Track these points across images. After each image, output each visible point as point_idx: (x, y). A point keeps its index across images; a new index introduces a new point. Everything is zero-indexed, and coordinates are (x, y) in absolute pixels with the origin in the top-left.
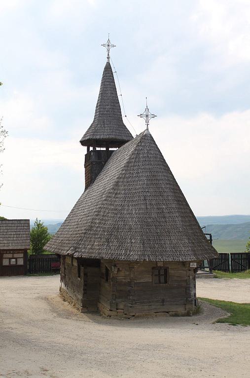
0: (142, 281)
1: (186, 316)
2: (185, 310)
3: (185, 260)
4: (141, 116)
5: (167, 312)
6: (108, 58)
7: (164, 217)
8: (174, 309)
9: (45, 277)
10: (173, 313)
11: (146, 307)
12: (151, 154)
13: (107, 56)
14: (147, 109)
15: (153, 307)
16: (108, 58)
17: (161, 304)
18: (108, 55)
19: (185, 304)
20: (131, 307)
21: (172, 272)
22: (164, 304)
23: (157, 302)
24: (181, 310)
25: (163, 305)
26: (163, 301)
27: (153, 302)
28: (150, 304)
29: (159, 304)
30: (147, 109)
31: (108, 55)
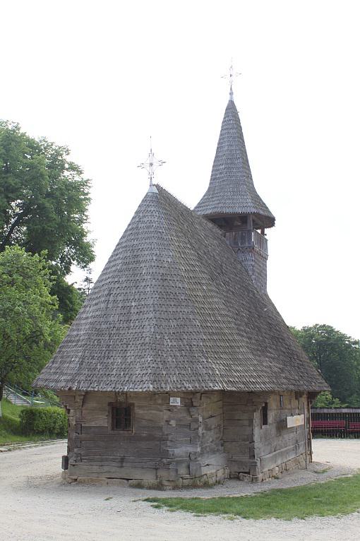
0: (93, 424)
1: (154, 489)
2: (157, 479)
3: (206, 389)
4: (141, 166)
5: (128, 480)
6: (231, 94)
7: (128, 321)
8: (137, 475)
9: (322, 438)
10: (134, 482)
11: (95, 468)
12: (143, 222)
13: (229, 91)
14: (151, 154)
15: (106, 469)
16: (231, 94)
17: (119, 464)
18: (231, 89)
19: (156, 469)
20: (74, 465)
21: (141, 412)
22: (124, 464)
23: (113, 460)
24: (149, 478)
25: (122, 467)
26: (122, 460)
27: (107, 460)
28: (103, 463)
29: (114, 464)
30: (151, 154)
31: (231, 89)
